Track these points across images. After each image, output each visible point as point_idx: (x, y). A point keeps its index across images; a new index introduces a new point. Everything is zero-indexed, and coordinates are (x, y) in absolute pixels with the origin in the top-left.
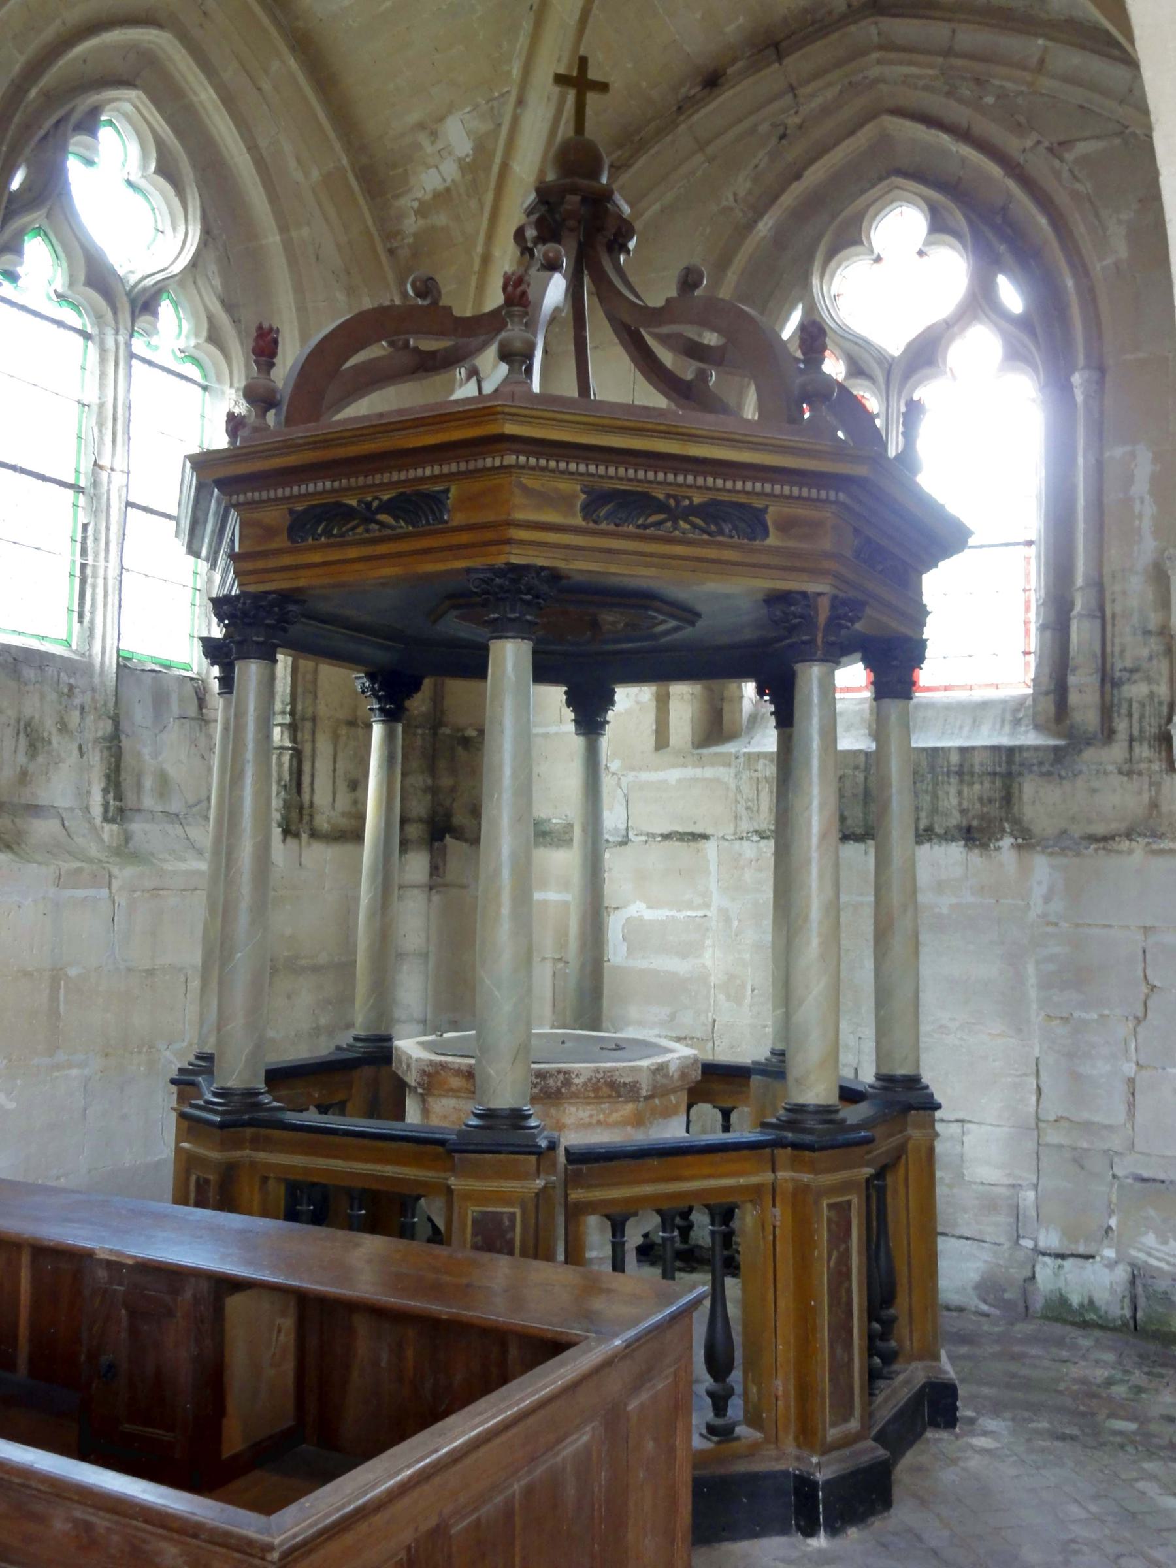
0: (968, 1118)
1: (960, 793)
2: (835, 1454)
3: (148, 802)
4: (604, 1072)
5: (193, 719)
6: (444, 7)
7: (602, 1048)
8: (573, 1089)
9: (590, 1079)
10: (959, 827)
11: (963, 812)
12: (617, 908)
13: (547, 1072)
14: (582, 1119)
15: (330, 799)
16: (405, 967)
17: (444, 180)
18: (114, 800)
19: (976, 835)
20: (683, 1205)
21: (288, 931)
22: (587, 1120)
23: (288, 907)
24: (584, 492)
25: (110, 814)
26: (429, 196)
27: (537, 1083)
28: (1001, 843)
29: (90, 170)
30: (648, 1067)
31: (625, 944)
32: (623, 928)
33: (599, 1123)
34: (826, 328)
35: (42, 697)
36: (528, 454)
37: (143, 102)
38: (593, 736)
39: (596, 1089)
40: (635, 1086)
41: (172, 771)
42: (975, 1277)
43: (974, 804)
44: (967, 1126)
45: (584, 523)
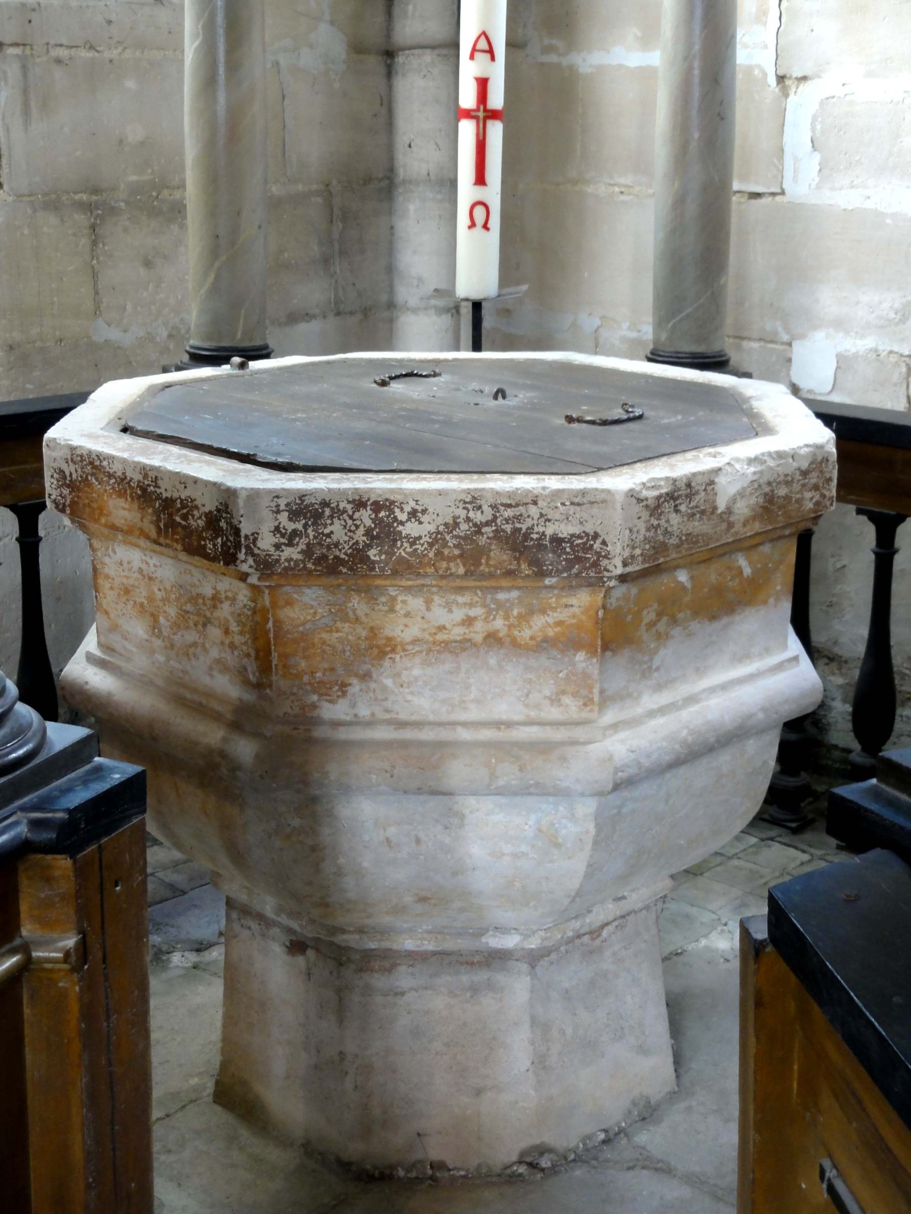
4: (493, 507)
7: (570, 419)
8: (403, 550)
12: (804, 78)
13: (325, 504)
14: (442, 628)
16: (412, 207)
21: (135, 133)
22: (458, 632)
23: (130, 84)
27: (295, 533)
30: (632, 494)
31: (817, 157)
32: (814, 118)
33: (492, 639)
40: (588, 548)
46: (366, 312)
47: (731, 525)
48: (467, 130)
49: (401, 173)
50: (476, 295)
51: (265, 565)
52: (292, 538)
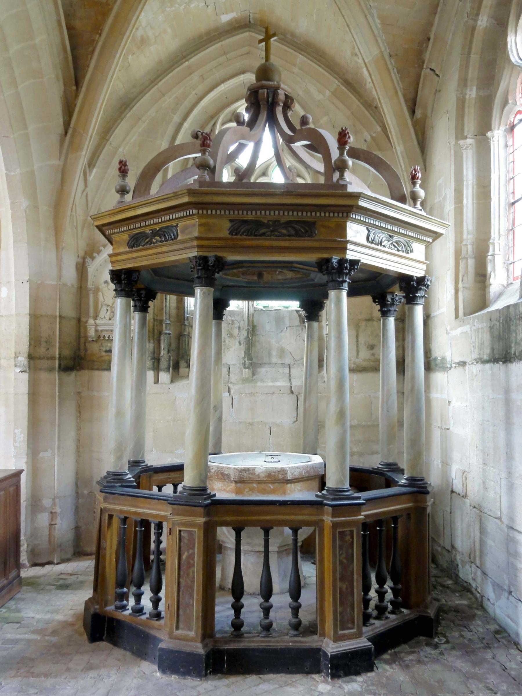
3: (274, 360)
18: (248, 360)
25: (247, 366)
34: (402, 90)
38: (385, 318)
39: (218, 475)
40: (229, 476)
47: (259, 477)
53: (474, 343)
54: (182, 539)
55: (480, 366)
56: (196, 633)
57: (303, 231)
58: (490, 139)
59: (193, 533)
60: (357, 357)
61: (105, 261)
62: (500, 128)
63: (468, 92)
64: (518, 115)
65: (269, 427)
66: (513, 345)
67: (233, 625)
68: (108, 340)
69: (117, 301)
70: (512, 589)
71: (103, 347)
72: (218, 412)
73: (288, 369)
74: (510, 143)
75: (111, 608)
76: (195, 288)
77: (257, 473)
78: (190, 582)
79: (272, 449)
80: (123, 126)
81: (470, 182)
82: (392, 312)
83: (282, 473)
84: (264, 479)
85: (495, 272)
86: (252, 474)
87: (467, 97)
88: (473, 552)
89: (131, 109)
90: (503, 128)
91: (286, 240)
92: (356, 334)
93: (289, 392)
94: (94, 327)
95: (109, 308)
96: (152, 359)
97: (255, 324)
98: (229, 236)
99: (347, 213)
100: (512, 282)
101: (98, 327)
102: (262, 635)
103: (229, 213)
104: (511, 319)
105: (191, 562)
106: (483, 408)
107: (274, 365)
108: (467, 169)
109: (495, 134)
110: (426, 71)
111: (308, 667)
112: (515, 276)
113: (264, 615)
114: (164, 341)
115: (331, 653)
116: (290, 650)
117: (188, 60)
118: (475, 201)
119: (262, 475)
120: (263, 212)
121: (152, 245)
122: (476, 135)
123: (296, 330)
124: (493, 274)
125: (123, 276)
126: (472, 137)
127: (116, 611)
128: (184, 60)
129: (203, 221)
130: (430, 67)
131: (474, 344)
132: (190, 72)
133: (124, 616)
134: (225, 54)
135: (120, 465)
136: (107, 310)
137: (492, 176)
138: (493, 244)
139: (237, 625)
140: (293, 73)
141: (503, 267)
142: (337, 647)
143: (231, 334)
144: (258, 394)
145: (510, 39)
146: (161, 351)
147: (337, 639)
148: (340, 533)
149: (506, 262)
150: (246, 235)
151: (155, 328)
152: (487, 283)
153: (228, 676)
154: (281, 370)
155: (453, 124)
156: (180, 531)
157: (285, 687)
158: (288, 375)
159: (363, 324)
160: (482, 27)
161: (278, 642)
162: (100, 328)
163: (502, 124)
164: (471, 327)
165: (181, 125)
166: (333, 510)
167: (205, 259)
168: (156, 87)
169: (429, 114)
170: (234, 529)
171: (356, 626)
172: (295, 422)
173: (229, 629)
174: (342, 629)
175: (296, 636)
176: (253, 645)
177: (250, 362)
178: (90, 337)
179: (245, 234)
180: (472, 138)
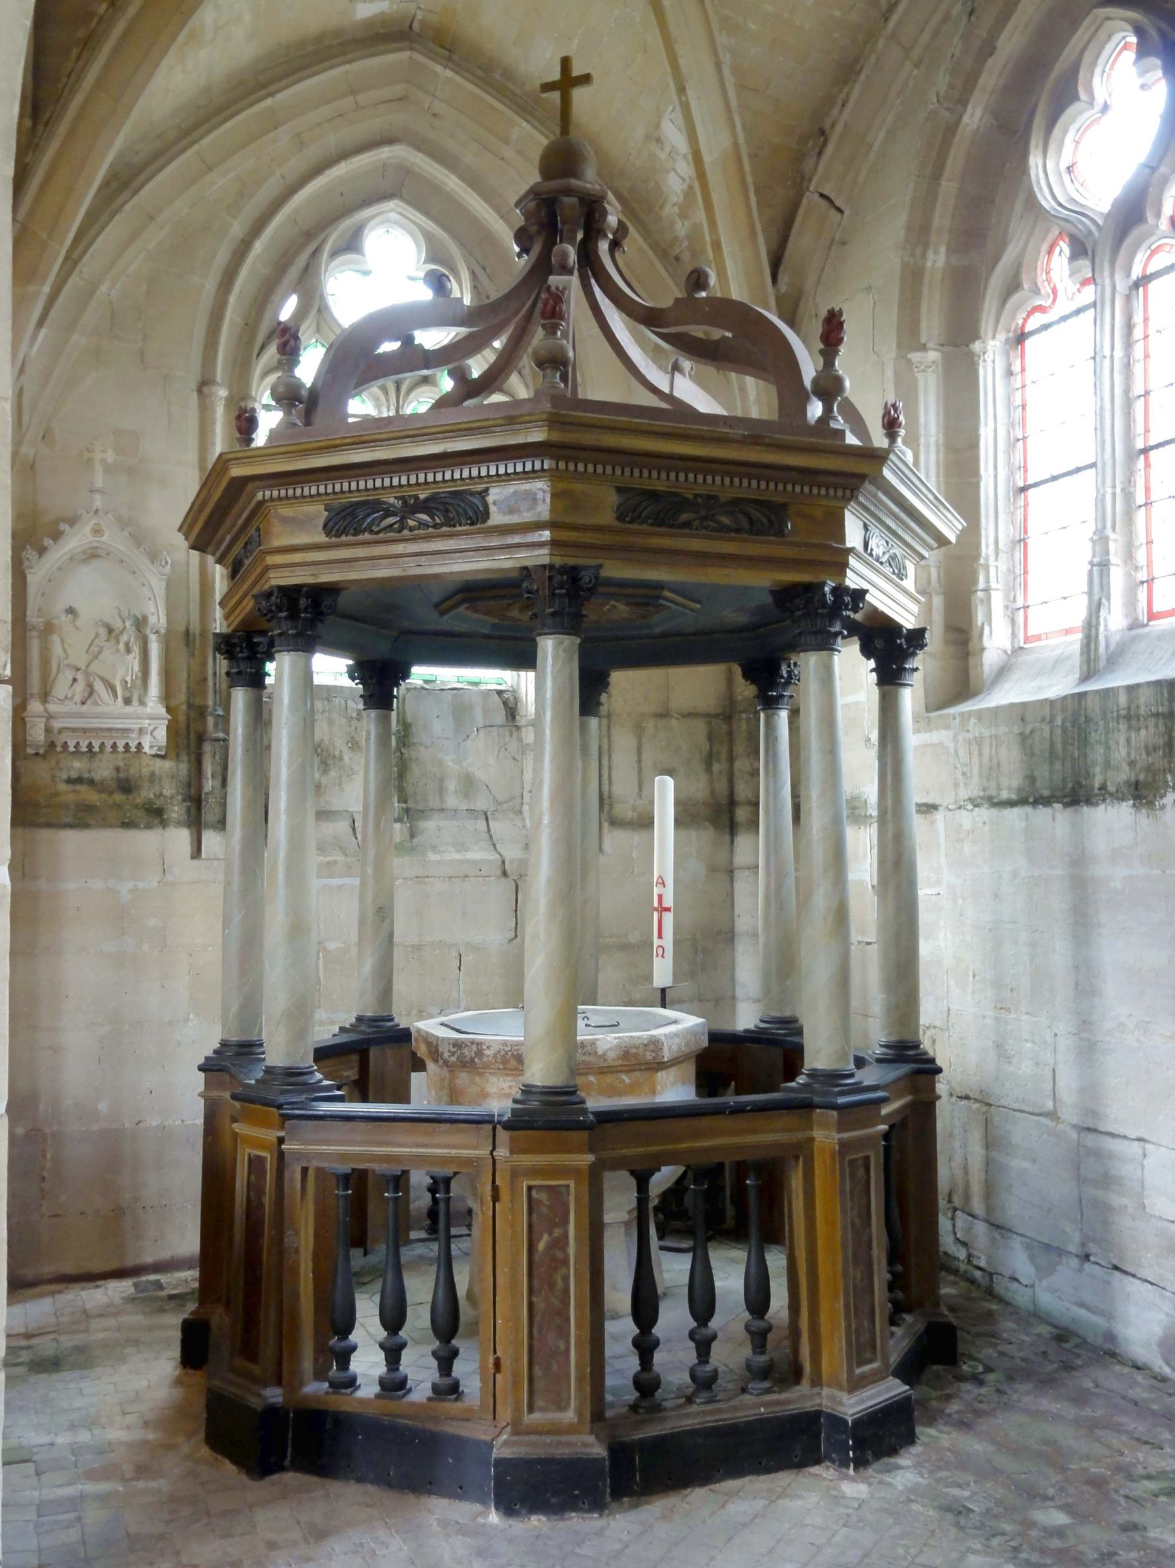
0: (1147, 1138)
1: (1128, 741)
2: (526, 1438)
3: (452, 801)
5: (501, 726)
6: (613, 25)
8: (485, 1059)
9: (499, 1052)
10: (1128, 783)
11: (1132, 764)
15: (636, 789)
17: (684, 180)
18: (399, 802)
19: (1144, 792)
20: (396, 1170)
22: (507, 1091)
24: (326, 510)
26: (681, 199)
27: (454, 1052)
28: (1164, 801)
29: (371, 275)
35: (331, 722)
36: (270, 487)
37: (405, 209)
38: (770, 711)
39: (505, 1061)
41: (479, 774)
42: (1158, 1330)
43: (1140, 755)
44: (1147, 1146)
45: (327, 539)
46: (718, 1001)
47: (606, 1060)
48: (656, 915)
49: (737, 930)
50: (662, 986)
51: (446, 1063)
52: (453, 1054)
53: (966, 765)
54: (535, 1207)
55: (985, 813)
56: (580, 1414)
57: (765, 521)
58: (979, 356)
59: (563, 1190)
60: (640, 797)
61: (71, 559)
62: (997, 336)
63: (930, 255)
64: (1037, 315)
65: (457, 954)
66: (1097, 770)
67: (638, 1383)
68: (74, 752)
69: (807, 663)
70: (1092, 1248)
71: (61, 769)
72: (387, 921)
73: (485, 822)
74: (1016, 367)
75: (315, 1388)
76: (538, 638)
77: (600, 1052)
78: (557, 1302)
79: (463, 1004)
80: (114, 231)
81: (932, 440)
82: (786, 699)
83: (651, 1047)
84: (616, 1063)
85: (990, 624)
86: (590, 1054)
87: (929, 264)
88: (960, 1189)
89: (136, 192)
90: (1002, 337)
91: (731, 540)
92: (636, 745)
93: (499, 873)
94: (44, 720)
95: (80, 676)
96: (184, 800)
97: (409, 720)
98: (617, 524)
99: (852, 490)
100: (1022, 644)
101: (52, 721)
102: (702, 1400)
103: (659, 478)
104: (1088, 720)
105: (560, 1255)
106: (996, 896)
107: (453, 813)
108: (926, 411)
109: (989, 348)
110: (810, 199)
111: (798, 1453)
112: (1029, 634)
113: (699, 1356)
114: (214, 757)
115: (852, 1415)
116: (763, 1422)
117: (271, 95)
118: (941, 479)
119: (611, 1055)
120: (691, 476)
121: (406, 532)
122: (942, 345)
123: (499, 734)
124: (986, 628)
125: (303, 602)
126: (937, 347)
127: (335, 1393)
128: (262, 93)
129: (561, 486)
130: (821, 191)
131: (965, 769)
132: (274, 122)
133: (362, 1401)
134: (353, 92)
135: (302, 1051)
136: (75, 680)
137: (982, 431)
138: (987, 568)
139: (646, 1385)
140: (502, 159)
141: (1005, 615)
142: (858, 1403)
143: (357, 742)
144: (431, 880)
145: (1035, 161)
146: (204, 781)
147: (856, 1384)
148: (852, 1162)
149: (1011, 605)
150: (652, 525)
151: (192, 726)
152: (972, 646)
153: (646, 1498)
154: (470, 824)
155: (890, 318)
156: (530, 1188)
157: (780, 1501)
158: (486, 836)
159: (650, 724)
160: (969, 128)
161: (735, 1409)
162: (57, 724)
163: (1000, 327)
164: (955, 736)
165: (245, 246)
166: (839, 1116)
167: (573, 574)
168: (196, 147)
169: (809, 284)
170: (632, 1173)
171: (879, 1355)
172: (511, 940)
173: (632, 1395)
174: (860, 1364)
175: (768, 1391)
176: (689, 1423)
177: (404, 806)
178: (31, 746)
179: (650, 521)
180: (936, 350)
